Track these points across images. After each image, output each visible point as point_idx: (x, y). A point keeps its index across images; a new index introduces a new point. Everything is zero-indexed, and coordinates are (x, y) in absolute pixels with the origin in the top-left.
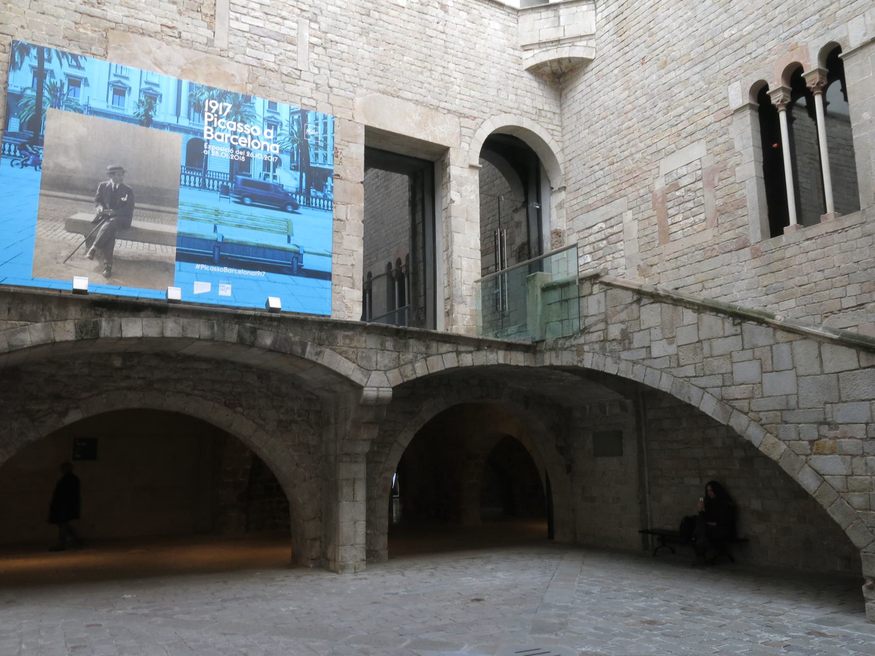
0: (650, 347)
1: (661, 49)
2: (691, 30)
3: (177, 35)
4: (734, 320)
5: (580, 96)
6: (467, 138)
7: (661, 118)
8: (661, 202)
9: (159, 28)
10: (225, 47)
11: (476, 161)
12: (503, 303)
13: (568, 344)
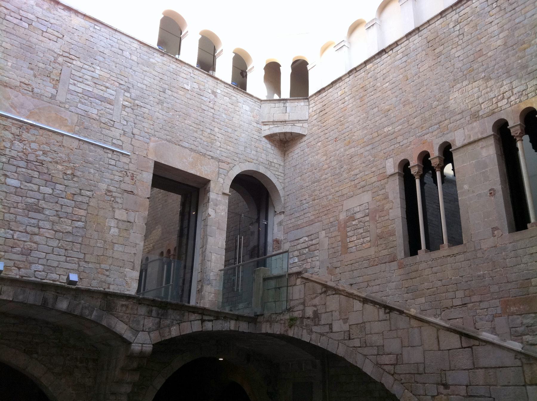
0: (332, 324)
1: (347, 134)
2: (365, 124)
3: (30, 90)
4: (385, 310)
5: (297, 156)
6: (223, 175)
7: (345, 175)
8: (343, 227)
9: (18, 84)
10: (63, 101)
11: (227, 191)
12: (238, 285)
13: (278, 318)
